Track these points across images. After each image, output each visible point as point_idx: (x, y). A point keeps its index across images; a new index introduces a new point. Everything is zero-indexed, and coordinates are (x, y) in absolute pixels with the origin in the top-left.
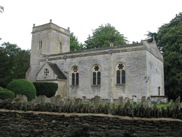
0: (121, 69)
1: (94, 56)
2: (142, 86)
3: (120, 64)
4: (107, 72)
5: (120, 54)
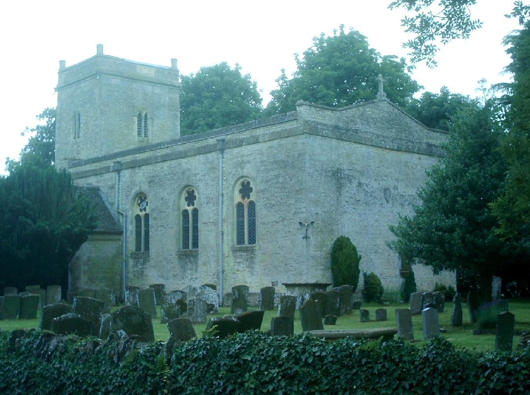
0: (246, 199)
1: (183, 160)
5: (245, 150)
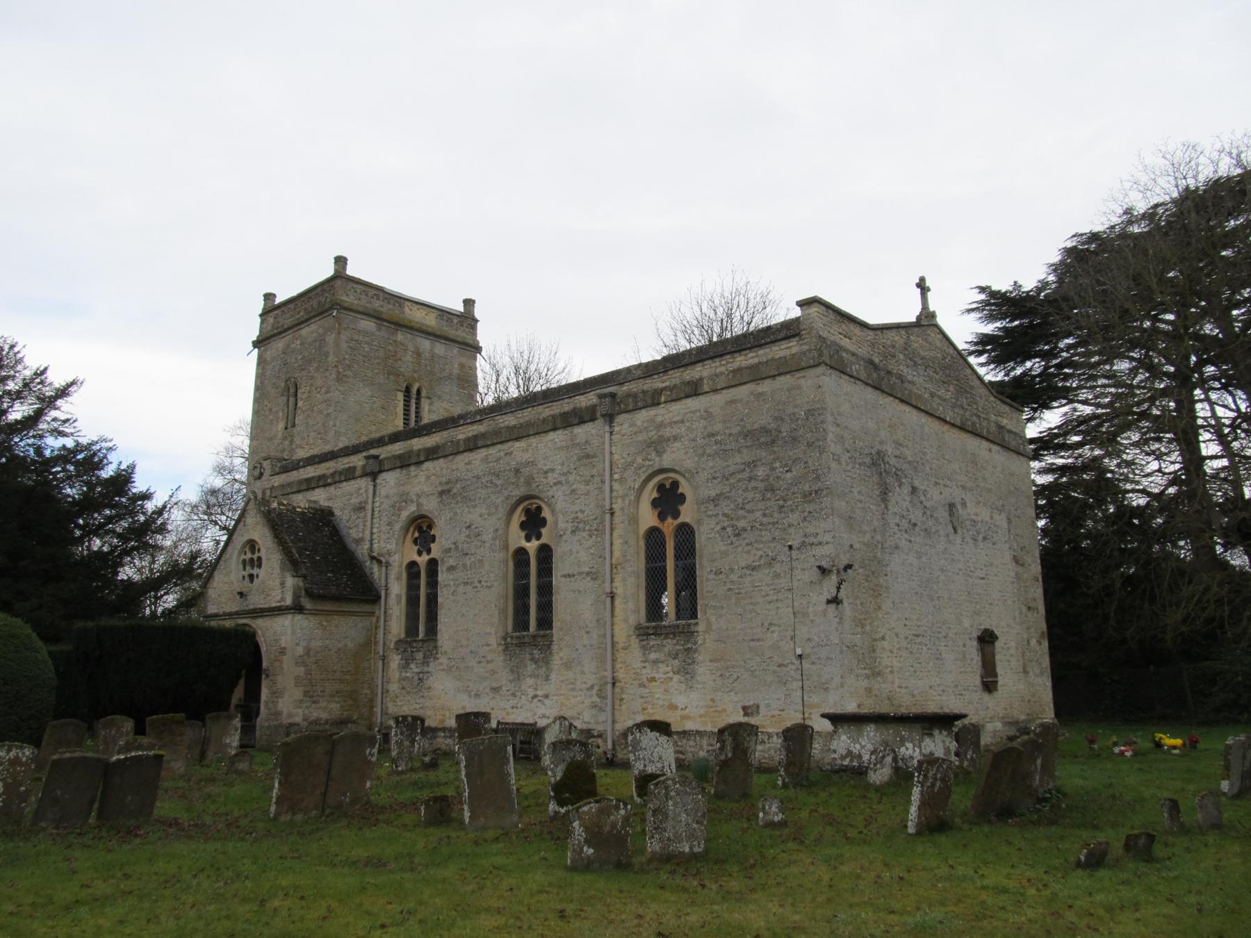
0: (670, 520)
1: (517, 444)
2: (803, 632)
3: (661, 487)
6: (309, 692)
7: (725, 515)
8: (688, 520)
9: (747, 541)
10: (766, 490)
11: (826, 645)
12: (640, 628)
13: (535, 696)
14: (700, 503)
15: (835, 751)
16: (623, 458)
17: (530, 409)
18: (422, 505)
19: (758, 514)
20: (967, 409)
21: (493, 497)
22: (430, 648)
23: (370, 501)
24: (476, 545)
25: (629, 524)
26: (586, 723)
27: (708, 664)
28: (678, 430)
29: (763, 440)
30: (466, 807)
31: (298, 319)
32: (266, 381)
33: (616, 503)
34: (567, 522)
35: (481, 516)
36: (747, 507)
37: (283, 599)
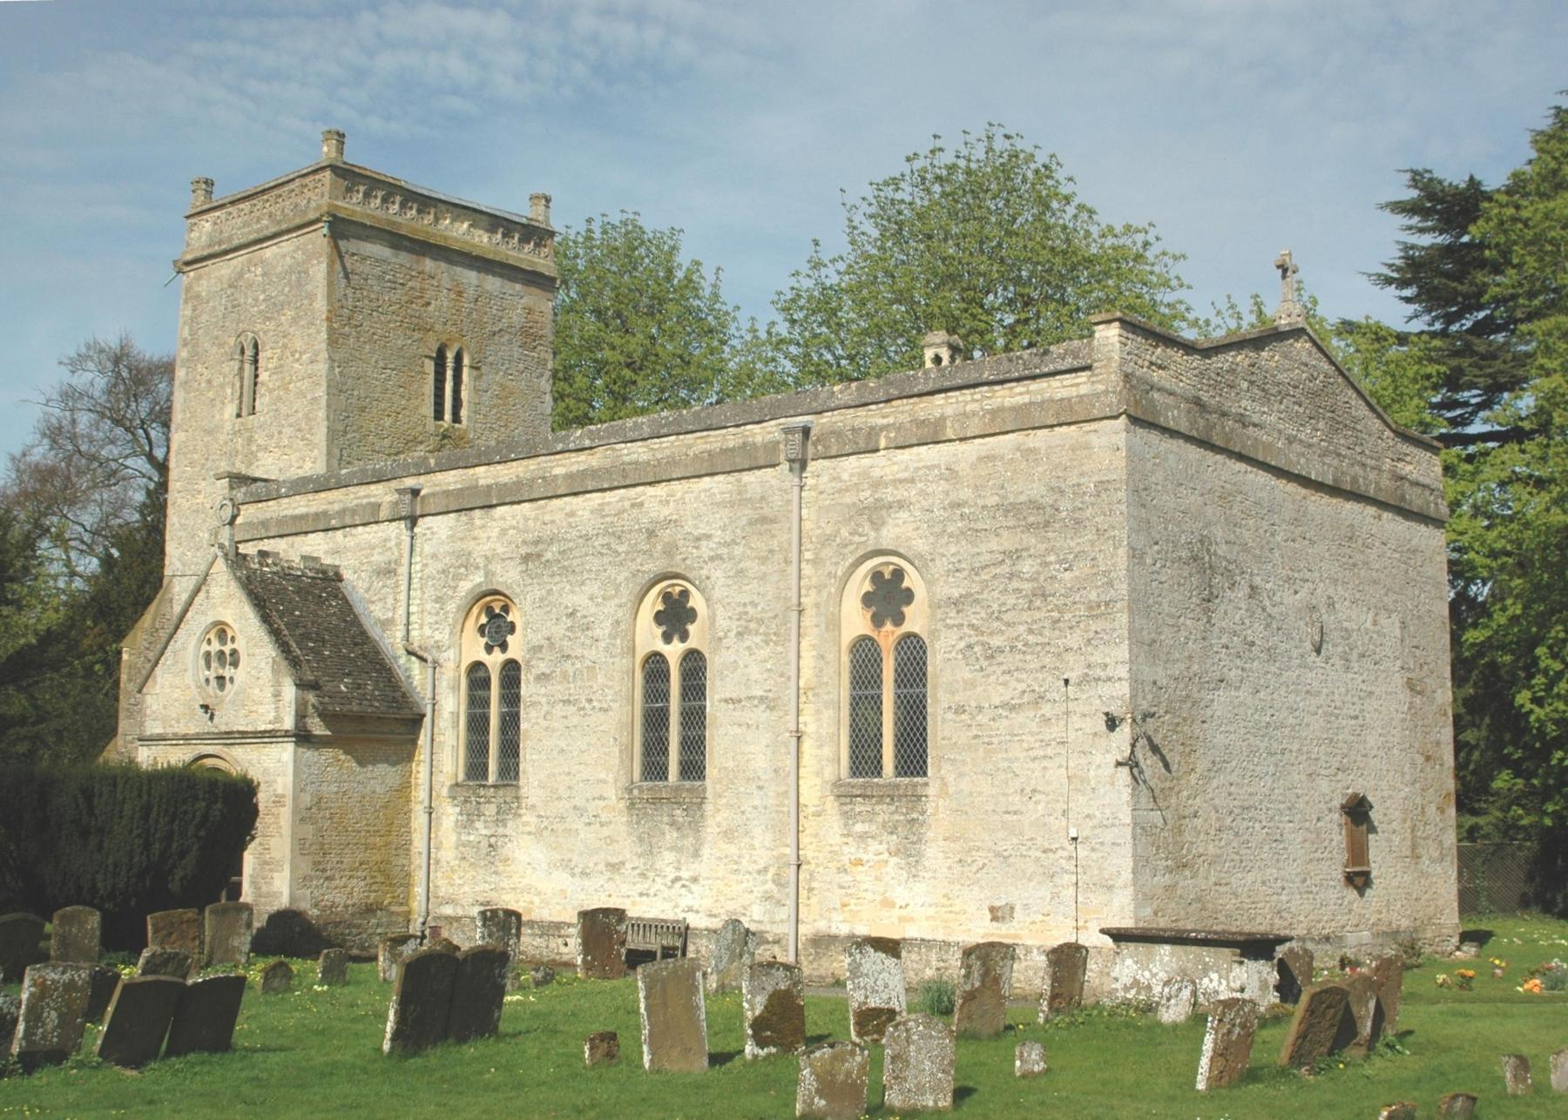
0: (889, 626)
1: (650, 490)
2: (1080, 803)
3: (877, 576)
4: (765, 652)
5: (886, 464)
6: (320, 863)
7: (971, 626)
8: (916, 630)
9: (1004, 667)
10: (1034, 595)
11: (1113, 825)
12: (841, 786)
13: (678, 879)
14: (935, 606)
15: (1117, 980)
16: (819, 527)
17: (673, 438)
18: (493, 574)
19: (1022, 628)
20: (1344, 457)
21: (612, 571)
22: (508, 799)
23: (405, 561)
24: (583, 644)
25: (827, 629)
26: (755, 921)
27: (942, 843)
28: (906, 493)
29: (1031, 519)
30: (645, 1048)
31: (257, 231)
32: (201, 332)
33: (806, 596)
34: (730, 618)
35: (591, 599)
36: (1006, 617)
37: (278, 719)
